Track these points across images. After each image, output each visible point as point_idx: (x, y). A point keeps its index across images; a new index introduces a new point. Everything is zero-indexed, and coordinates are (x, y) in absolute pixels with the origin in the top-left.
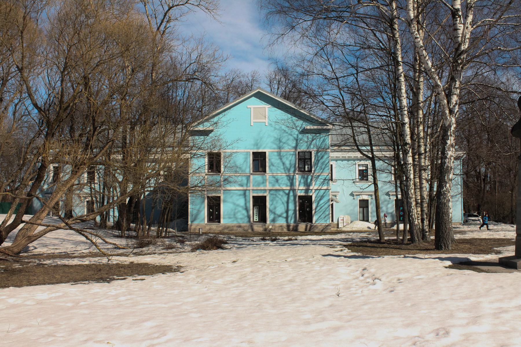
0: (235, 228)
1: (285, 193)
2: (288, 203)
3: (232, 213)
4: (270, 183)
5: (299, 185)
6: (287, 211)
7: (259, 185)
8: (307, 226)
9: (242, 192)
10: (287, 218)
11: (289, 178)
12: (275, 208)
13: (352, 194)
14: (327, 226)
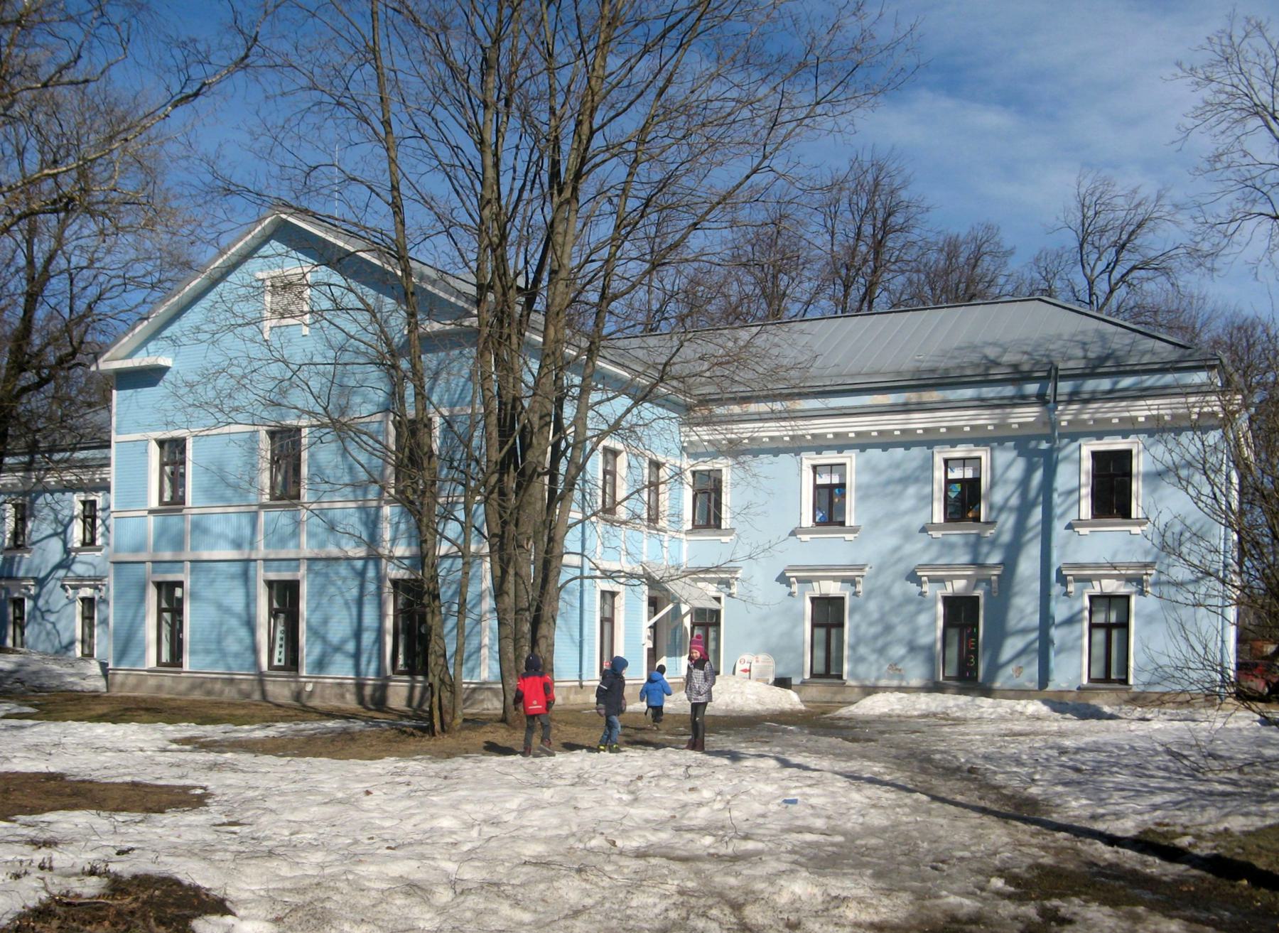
0: (218, 686)
1: (353, 568)
2: (360, 602)
3: (214, 636)
4: (311, 535)
5: (394, 540)
6: (358, 634)
7: (282, 542)
8: (412, 689)
9: (236, 568)
10: (357, 656)
11: (364, 516)
12: (325, 621)
13: (783, 579)
14: (474, 690)
